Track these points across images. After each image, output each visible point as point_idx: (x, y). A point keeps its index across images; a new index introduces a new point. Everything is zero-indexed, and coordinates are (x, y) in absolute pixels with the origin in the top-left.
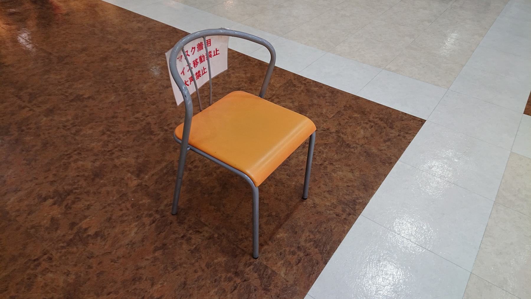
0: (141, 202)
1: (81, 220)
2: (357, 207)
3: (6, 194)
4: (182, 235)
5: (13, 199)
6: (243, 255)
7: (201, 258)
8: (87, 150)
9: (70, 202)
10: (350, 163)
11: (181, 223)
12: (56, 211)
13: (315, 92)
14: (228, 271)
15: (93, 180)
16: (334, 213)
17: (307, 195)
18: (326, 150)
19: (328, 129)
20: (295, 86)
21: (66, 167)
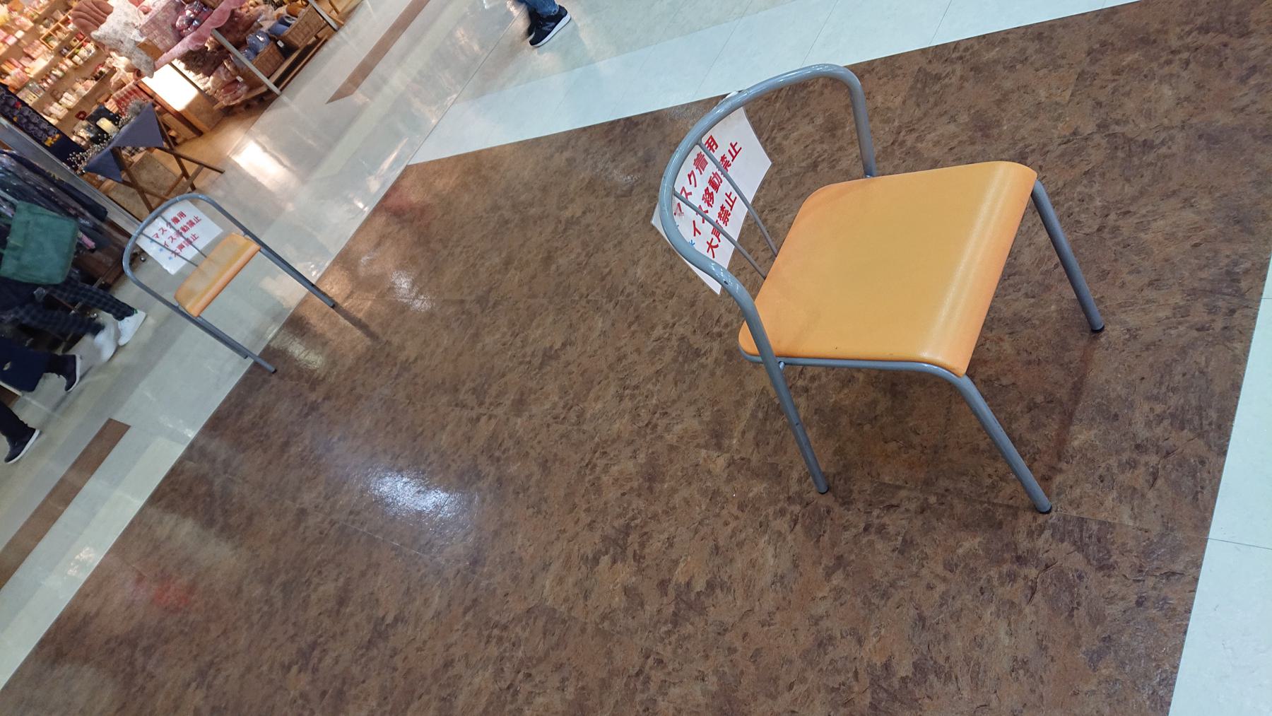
0: (751, 495)
1: (670, 571)
2: (1244, 285)
3: (533, 578)
4: (862, 526)
5: (548, 581)
6: (1015, 516)
7: (926, 557)
8: (614, 441)
9: (636, 546)
10: (1173, 185)
11: (846, 502)
12: (625, 573)
13: (996, 62)
14: (1000, 562)
15: (651, 489)
16: (1191, 327)
17: (1099, 320)
18: (1097, 187)
19: (1074, 134)
20: (938, 78)
21: (596, 487)
